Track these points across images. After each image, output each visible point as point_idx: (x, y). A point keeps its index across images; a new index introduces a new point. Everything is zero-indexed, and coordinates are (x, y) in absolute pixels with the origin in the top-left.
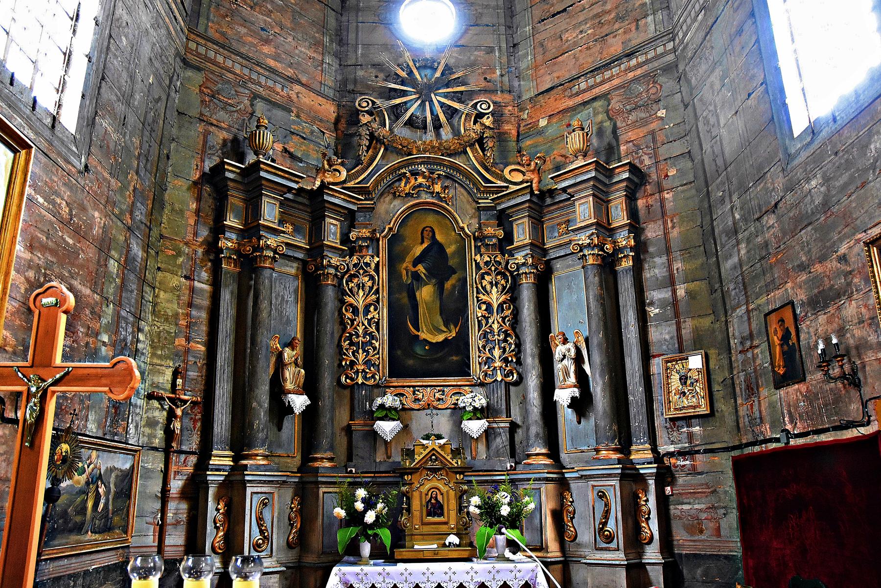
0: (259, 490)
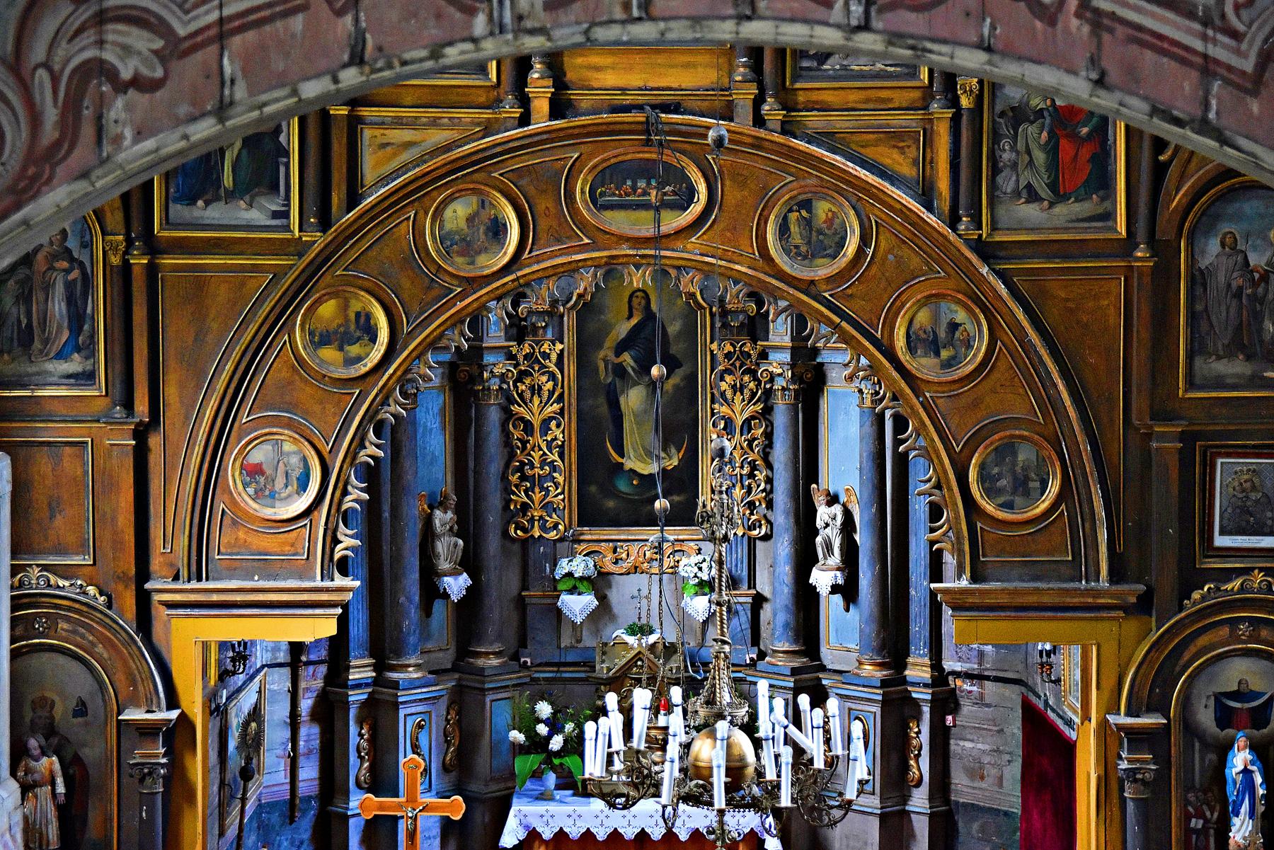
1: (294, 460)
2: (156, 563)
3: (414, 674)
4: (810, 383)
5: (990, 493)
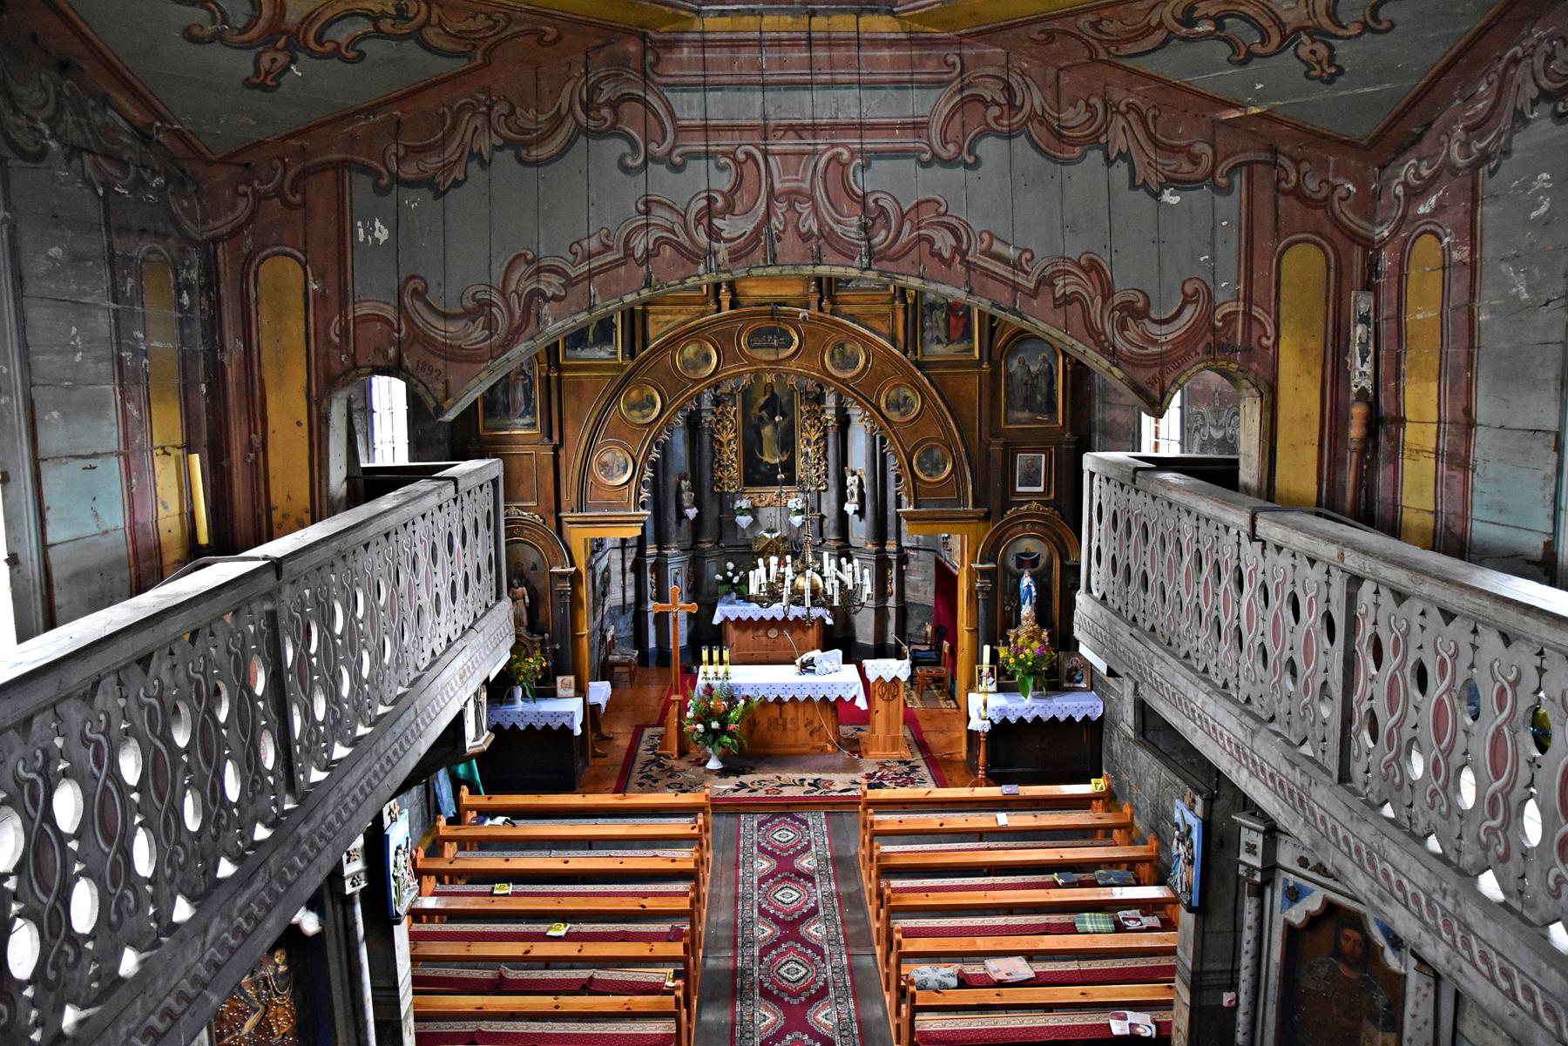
2: (563, 504)
3: (674, 551)
4: (844, 423)
5: (921, 470)
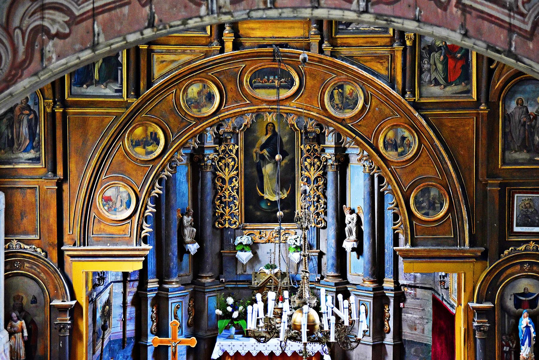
0: (175, 301)
1: (125, 195)
